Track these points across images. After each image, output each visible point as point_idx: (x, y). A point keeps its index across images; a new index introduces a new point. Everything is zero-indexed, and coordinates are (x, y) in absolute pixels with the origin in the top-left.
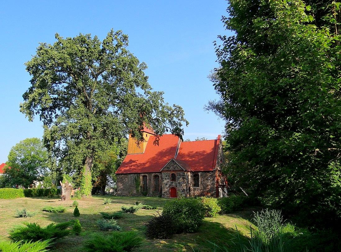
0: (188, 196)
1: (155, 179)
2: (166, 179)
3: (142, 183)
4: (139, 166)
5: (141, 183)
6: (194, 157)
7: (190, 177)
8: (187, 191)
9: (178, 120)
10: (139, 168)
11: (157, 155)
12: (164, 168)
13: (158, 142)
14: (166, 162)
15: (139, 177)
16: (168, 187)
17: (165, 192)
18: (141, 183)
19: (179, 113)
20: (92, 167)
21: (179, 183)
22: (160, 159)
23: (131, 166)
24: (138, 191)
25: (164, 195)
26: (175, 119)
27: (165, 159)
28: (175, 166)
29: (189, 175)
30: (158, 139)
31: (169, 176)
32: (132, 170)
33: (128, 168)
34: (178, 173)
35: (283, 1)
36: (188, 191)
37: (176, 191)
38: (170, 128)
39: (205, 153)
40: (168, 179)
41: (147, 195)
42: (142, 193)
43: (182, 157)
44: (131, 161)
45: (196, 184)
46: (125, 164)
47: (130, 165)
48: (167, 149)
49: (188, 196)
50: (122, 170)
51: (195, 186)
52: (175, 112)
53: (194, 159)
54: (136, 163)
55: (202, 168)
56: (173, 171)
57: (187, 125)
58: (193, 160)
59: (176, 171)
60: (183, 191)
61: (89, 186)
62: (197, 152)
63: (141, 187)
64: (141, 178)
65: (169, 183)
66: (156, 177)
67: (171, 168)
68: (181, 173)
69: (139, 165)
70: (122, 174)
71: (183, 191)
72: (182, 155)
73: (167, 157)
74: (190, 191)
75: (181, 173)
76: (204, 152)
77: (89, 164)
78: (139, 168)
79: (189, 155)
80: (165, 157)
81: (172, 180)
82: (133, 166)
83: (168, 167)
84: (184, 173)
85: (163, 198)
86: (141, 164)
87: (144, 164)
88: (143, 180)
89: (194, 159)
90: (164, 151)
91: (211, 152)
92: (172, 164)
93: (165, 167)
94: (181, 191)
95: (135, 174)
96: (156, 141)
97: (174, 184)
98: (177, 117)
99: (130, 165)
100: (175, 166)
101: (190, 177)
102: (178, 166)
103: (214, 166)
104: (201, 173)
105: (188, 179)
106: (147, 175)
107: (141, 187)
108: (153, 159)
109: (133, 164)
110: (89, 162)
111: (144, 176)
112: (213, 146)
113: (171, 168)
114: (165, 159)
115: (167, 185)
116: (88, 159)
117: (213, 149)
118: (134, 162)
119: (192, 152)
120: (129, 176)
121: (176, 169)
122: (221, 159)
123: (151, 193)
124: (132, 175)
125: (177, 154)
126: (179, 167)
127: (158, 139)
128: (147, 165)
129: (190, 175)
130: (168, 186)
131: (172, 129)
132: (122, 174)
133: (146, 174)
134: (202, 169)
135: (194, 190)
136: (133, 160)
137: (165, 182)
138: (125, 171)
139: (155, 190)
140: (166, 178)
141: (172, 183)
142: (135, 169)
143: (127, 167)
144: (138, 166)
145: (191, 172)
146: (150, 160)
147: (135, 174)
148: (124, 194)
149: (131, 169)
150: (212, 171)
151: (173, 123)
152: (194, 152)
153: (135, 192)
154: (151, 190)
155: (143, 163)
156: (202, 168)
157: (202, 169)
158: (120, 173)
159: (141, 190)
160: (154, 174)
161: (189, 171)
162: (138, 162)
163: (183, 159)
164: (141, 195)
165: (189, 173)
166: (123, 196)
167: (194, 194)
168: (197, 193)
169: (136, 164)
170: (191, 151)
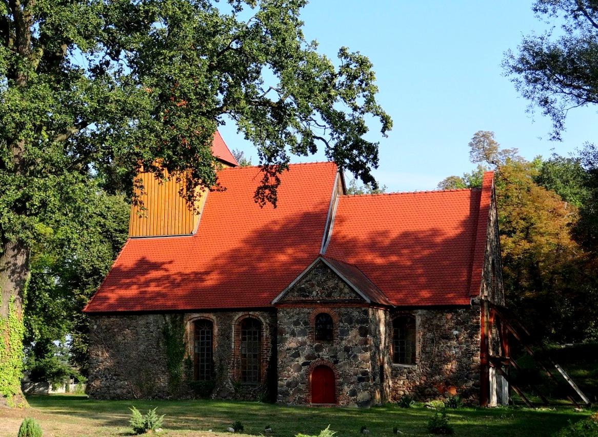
0: (378, 396)
1: (244, 333)
2: (293, 334)
3: (190, 349)
4: (179, 285)
5: (190, 347)
6: (393, 253)
7: (382, 328)
8: (374, 379)
9: (350, 111)
10: (179, 292)
11: (246, 241)
12: (286, 295)
13: (274, 193)
14: (288, 272)
15: (181, 326)
16: (304, 364)
17: (289, 385)
18: (190, 347)
19: (356, 82)
20: (27, 284)
21: (347, 349)
22: (260, 259)
23: (147, 283)
24: (174, 379)
25: (286, 394)
26: (340, 106)
27: (282, 258)
28: (331, 284)
29: (380, 320)
30: (272, 181)
31: (306, 323)
32: (151, 299)
33: (133, 292)
34: (343, 310)
35: (25, 3)
36: (378, 378)
37: (334, 378)
38: (327, 137)
39: (439, 239)
40: (303, 333)
41: (213, 396)
42: (192, 386)
43: (347, 254)
44: (144, 266)
45: (403, 354)
46: (118, 277)
47: (142, 279)
48: (290, 221)
49: (378, 396)
50: (107, 298)
51: (396, 362)
52: (343, 79)
53: (394, 258)
54: (166, 270)
55: (425, 294)
56: (324, 303)
57: (383, 131)
58: (392, 265)
59: (335, 302)
60: (360, 380)
61: (15, 360)
62: (405, 235)
63: (188, 362)
64: (189, 327)
65: (307, 350)
66: (249, 327)
67: (316, 293)
68: (355, 314)
69: (179, 279)
70: (108, 314)
71: (360, 380)
72: (348, 246)
73: (290, 251)
74: (382, 380)
75: (355, 314)
76: (435, 232)
77: (13, 272)
78: (179, 292)
79: (373, 245)
80: (281, 250)
81: (318, 339)
82: (153, 284)
83: (301, 290)
84: (366, 313)
85: (284, 405)
86: (186, 278)
87: (198, 276)
88: (196, 339)
89: (394, 258)
90: (277, 228)
91: (462, 234)
92: (322, 278)
93: (292, 289)
94: (354, 379)
95: (163, 313)
96: (266, 187)
97: (325, 354)
98: (348, 98)
99: (142, 279)
100: (331, 284)
101: (382, 328)
102: (341, 285)
103: (470, 289)
104: (425, 311)
105: (376, 335)
106: (212, 317)
107: (188, 362)
108: (234, 256)
109: (154, 274)
110: (15, 265)
111: (198, 324)
112: (464, 210)
113: (316, 293)
114: (282, 258)
115: (297, 355)
116: (11, 253)
117: (464, 223)
118: (156, 266)
119: (385, 233)
120: (142, 321)
121: (336, 296)
122: (493, 261)
123: (229, 385)
124: (151, 318)
125: (329, 239)
126: (346, 290)
127: (272, 181)
128: (212, 280)
129: (383, 320)
130: (301, 360)
131: (332, 144)
132: (108, 314)
133: (206, 315)
134: (423, 299)
135: (395, 374)
136: (152, 258)
137: (291, 343)
138: (122, 300)
139: (244, 376)
140: (297, 329)
141: (318, 349)
142: (163, 296)
143: (128, 286)
144: (174, 284)
145: (388, 309)
146: (220, 262)
147: (163, 313)
148: (118, 391)
149: (148, 296)
150: (467, 307)
151: (335, 120)
152: (394, 234)
153: (162, 382)
154: (231, 375)
155: (196, 274)
156: (425, 294)
157: (428, 299)
158: (102, 308)
159: (188, 375)
160: (241, 314)
161: (382, 306)
162: (173, 269)
163: (352, 261)
164: (187, 394)
165: (381, 314)
166: (113, 399)
167: (395, 390)
168: (403, 386)
169: (168, 277)
170: (381, 228)
